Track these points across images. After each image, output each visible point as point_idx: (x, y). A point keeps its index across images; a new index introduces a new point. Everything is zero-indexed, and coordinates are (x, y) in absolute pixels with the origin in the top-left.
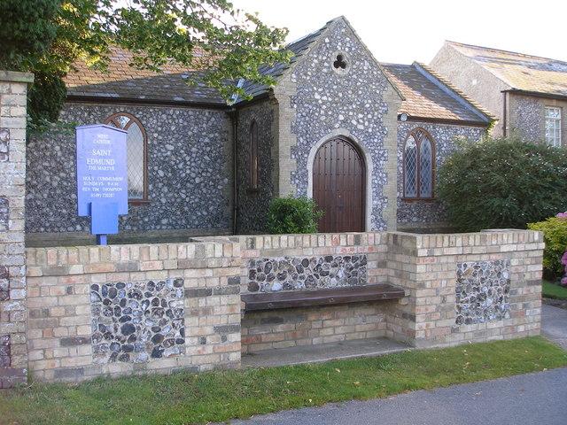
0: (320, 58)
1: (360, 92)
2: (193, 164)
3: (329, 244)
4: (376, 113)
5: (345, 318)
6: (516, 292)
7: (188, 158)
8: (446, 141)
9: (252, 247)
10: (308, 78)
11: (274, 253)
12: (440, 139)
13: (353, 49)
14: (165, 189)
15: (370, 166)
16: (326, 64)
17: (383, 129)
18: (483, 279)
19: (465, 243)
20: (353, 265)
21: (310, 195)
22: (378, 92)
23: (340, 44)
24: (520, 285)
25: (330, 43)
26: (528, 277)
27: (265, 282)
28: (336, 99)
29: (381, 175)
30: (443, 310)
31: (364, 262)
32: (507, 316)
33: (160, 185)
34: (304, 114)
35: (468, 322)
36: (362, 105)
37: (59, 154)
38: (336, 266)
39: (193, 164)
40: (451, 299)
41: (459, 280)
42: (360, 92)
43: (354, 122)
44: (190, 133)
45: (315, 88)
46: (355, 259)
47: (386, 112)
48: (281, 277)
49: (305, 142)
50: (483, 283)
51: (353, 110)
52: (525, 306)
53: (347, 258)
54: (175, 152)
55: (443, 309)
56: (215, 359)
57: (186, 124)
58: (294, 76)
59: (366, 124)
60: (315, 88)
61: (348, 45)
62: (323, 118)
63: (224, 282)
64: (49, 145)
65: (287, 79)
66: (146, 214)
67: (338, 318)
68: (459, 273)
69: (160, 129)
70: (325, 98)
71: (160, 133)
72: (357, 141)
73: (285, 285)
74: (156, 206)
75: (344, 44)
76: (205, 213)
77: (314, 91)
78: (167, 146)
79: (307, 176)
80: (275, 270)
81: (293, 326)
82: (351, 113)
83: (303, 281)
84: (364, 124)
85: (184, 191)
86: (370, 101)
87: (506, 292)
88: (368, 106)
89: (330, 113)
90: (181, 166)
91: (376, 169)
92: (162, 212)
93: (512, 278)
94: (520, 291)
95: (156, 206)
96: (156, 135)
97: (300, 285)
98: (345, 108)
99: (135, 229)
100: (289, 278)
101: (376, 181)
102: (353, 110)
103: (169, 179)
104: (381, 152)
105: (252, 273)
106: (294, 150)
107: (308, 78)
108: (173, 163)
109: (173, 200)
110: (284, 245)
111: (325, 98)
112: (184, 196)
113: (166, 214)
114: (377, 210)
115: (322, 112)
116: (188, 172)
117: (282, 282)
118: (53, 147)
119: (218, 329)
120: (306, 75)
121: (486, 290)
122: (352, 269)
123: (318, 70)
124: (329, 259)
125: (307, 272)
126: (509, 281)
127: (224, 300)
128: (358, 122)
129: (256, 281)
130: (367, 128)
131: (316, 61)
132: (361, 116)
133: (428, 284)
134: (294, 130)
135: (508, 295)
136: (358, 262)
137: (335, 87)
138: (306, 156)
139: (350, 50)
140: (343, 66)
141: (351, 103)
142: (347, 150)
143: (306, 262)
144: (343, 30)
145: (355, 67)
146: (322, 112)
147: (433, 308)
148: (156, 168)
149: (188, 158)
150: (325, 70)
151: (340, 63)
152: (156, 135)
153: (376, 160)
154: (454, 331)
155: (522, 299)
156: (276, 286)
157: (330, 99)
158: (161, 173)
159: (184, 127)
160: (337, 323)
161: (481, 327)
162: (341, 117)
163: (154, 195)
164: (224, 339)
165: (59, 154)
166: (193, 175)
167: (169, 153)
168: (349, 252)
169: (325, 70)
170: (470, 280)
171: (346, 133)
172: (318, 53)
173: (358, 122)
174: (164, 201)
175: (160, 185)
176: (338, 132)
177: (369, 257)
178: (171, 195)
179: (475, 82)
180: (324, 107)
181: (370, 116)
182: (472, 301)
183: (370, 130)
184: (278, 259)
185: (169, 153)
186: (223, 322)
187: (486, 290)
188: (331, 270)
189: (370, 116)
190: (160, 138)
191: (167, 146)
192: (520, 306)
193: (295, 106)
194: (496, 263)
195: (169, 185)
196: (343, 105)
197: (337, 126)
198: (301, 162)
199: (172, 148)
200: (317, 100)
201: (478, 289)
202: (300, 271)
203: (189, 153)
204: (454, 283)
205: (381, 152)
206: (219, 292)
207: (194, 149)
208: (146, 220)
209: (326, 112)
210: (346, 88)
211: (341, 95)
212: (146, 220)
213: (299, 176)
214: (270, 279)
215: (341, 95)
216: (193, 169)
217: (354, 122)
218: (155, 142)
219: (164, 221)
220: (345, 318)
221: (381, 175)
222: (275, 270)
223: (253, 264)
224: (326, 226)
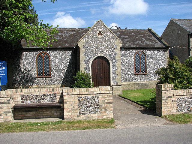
0: (93, 33)
1: (107, 42)
2: (64, 66)
3: (44, 91)
4: (113, 48)
5: (50, 111)
6: (102, 106)
7: (62, 64)
8: (150, 55)
9: (22, 92)
10: (89, 39)
11: (28, 93)
12: (148, 54)
13: (104, 29)
14: (56, 73)
15: (111, 65)
16: (95, 35)
17: (115, 53)
18: (88, 102)
19: (81, 91)
20: (52, 97)
21: (91, 74)
22: (113, 42)
23: (99, 28)
24: (104, 104)
25: (96, 28)
26: (106, 101)
27: (26, 101)
28: (99, 45)
29: (115, 67)
30: (74, 110)
31: (55, 96)
32: (99, 112)
33: (54, 72)
34: (88, 50)
35: (83, 114)
36: (108, 46)
37: (26, 64)
38: (47, 97)
39: (64, 66)
40: (77, 107)
41: (79, 102)
42: (107, 42)
43: (105, 52)
44: (63, 57)
45: (91, 42)
46: (53, 95)
47: (116, 48)
48: (30, 100)
49: (88, 59)
50: (88, 103)
51: (104, 48)
52: (105, 110)
53: (50, 95)
54: (59, 62)
55: (74, 110)
56: (4, 120)
57: (61, 54)
58: (84, 39)
59: (109, 52)
60: (91, 42)
61: (102, 28)
62: (94, 51)
63: (6, 101)
64: (23, 62)
65: (82, 40)
66: (50, 80)
67: (48, 111)
68: (79, 100)
69: (54, 56)
70: (95, 45)
71: (54, 57)
72: (106, 57)
73: (32, 102)
74: (53, 78)
75: (101, 28)
76: (68, 80)
77: (91, 43)
78: (56, 61)
79: (89, 69)
80: (28, 98)
81: (34, 113)
82: (104, 49)
83: (37, 101)
84: (108, 52)
85: (62, 73)
86: (110, 45)
87: (98, 105)
88: (110, 46)
89: (97, 49)
90: (60, 66)
91: (113, 66)
92: (55, 79)
93: (100, 101)
94: (103, 105)
95: (53, 78)
96: (53, 58)
97: (36, 102)
98: (102, 48)
99: (47, 84)
100: (32, 100)
101: (113, 69)
102: (104, 48)
103: (57, 70)
104: (115, 60)
105: (22, 99)
106: (85, 61)
107: (89, 39)
108: (58, 65)
109: (58, 76)
110: (31, 91)
111: (95, 45)
112: (61, 75)
113: (56, 80)
114: (113, 78)
115: (94, 49)
116: (63, 68)
117: (31, 101)
118: (24, 62)
119: (5, 112)
120: (88, 38)
121: (90, 105)
122: (52, 98)
123: (92, 37)
124: (44, 95)
125: (38, 99)
126: (99, 102)
127: (6, 105)
128: (106, 51)
129: (23, 100)
130: (109, 53)
131: (91, 34)
132: (107, 49)
133: (68, 103)
134: (85, 55)
135: (99, 107)
136: (54, 96)
137: (98, 41)
138: (89, 63)
139: (103, 30)
140: (102, 34)
141: (104, 46)
142: (102, 61)
143: (37, 96)
144: (101, 24)
145: (105, 35)
146: (94, 49)
147: (70, 109)
148: (53, 67)
149: (62, 64)
150: (95, 37)
151: (100, 33)
152: (53, 58)
153: (113, 63)
154: (78, 116)
155: (104, 108)
156: (29, 102)
157: (96, 45)
158: (55, 69)
159: (61, 55)
160: (48, 112)
161: (88, 116)
162: (101, 50)
163: (53, 75)
164: (6, 115)
165: (26, 64)
166: (64, 69)
167: (57, 63)
168: (50, 93)
169: (95, 37)
170: (83, 102)
171: (102, 55)
172: (92, 32)
173: (106, 51)
174: (55, 76)
175: (54, 72)
176: (99, 55)
177: (57, 95)
178: (58, 74)
179: (180, 32)
180: (95, 48)
181: (110, 49)
182: (85, 108)
183: (111, 54)
184: (29, 95)
185: (57, 63)
186: (6, 111)
187: (90, 105)
188: (45, 98)
189: (110, 49)
190: (54, 58)
191: (56, 61)
192: (104, 110)
193: (85, 48)
194: (93, 97)
195: (57, 72)
196: (101, 47)
197: (99, 53)
198: (87, 65)
199: (58, 61)
200: (92, 46)
201: (87, 105)
202: (36, 98)
203: (63, 62)
204: (77, 102)
205: (115, 60)
206: (5, 103)
207: (64, 61)
208: (51, 82)
209: (95, 49)
210: (102, 42)
211: (100, 44)
212: (51, 82)
213: (87, 68)
214: (27, 100)
215: (100, 44)
216: (64, 67)
217: (105, 52)
218: (53, 60)
219: (56, 82)
220: (50, 111)
221: (115, 67)
222: (28, 98)
223: (22, 96)
224: (97, 84)
